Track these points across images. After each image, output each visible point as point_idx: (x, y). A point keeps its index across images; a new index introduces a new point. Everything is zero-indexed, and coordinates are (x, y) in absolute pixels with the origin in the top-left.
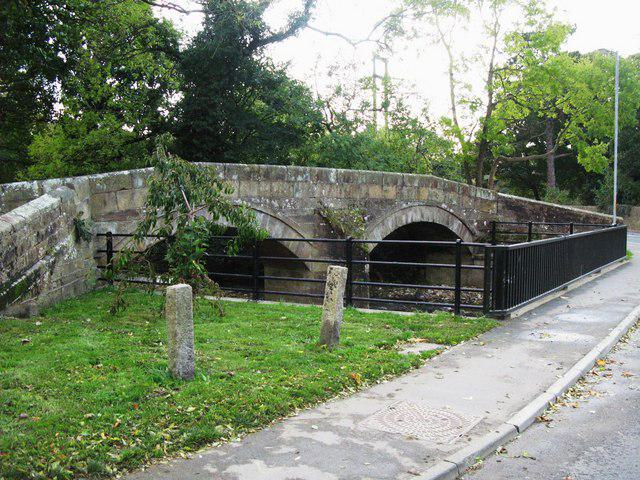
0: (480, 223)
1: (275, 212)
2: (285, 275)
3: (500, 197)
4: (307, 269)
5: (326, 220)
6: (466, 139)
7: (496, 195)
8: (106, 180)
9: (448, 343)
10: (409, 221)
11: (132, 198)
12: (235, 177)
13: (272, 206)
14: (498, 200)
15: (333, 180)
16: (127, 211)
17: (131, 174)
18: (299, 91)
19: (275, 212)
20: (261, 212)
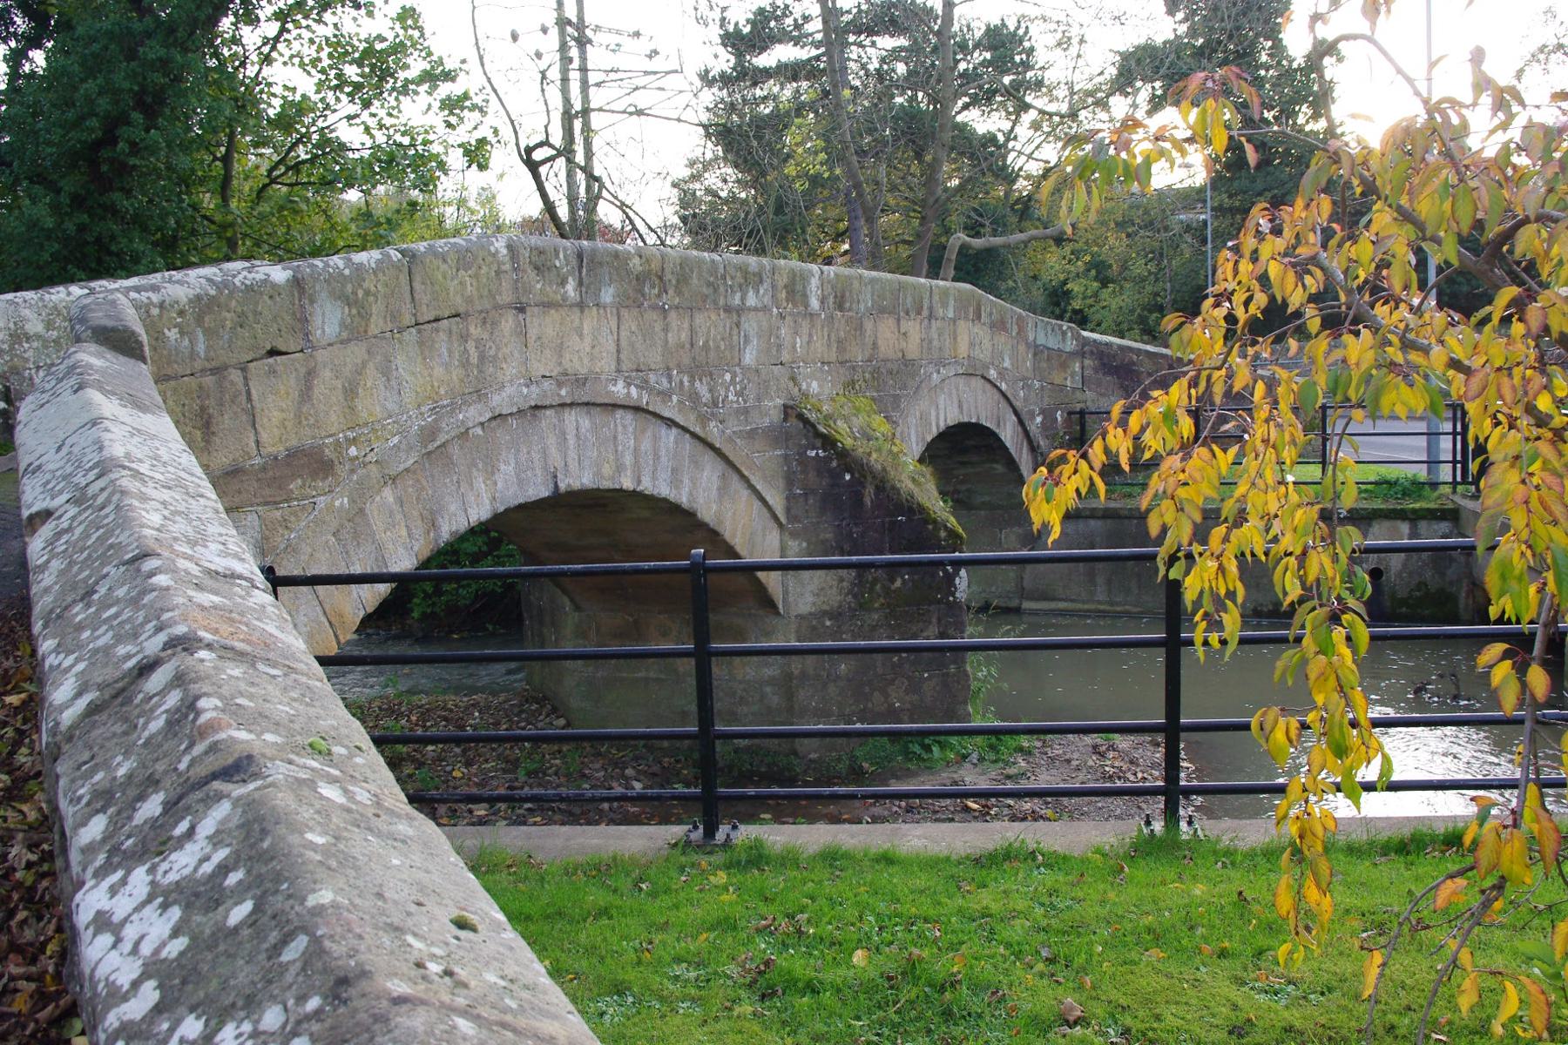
0: (1048, 414)
1: (703, 420)
2: (664, 634)
3: (1086, 341)
4: (767, 602)
5: (828, 442)
6: (689, 115)
7: (1078, 337)
8: (203, 306)
9: (295, 626)
10: (942, 426)
11: (306, 393)
12: (608, 295)
13: (694, 397)
14: (1085, 349)
15: (815, 303)
16: (293, 454)
17: (297, 283)
18: (1138, 48)
19: (703, 420)
20: (671, 423)
